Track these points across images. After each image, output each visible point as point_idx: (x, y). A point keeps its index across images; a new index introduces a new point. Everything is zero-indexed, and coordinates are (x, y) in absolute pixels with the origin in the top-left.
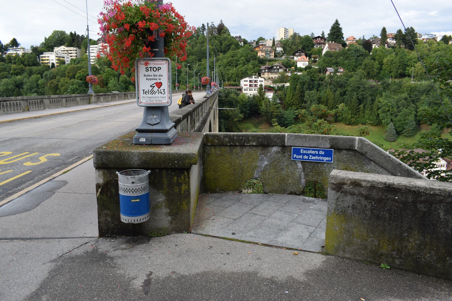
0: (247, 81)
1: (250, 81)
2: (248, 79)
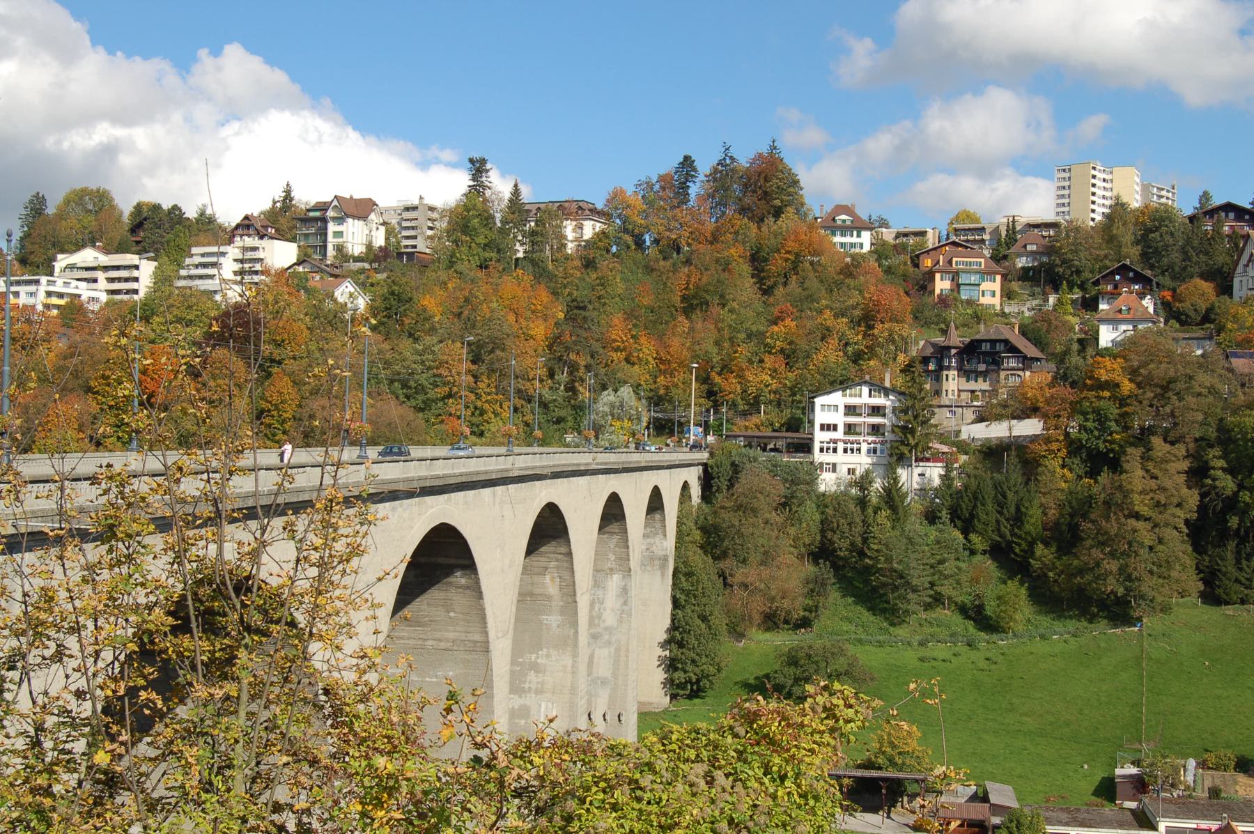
1: (851, 410)
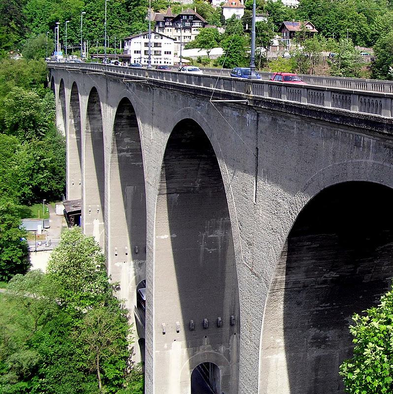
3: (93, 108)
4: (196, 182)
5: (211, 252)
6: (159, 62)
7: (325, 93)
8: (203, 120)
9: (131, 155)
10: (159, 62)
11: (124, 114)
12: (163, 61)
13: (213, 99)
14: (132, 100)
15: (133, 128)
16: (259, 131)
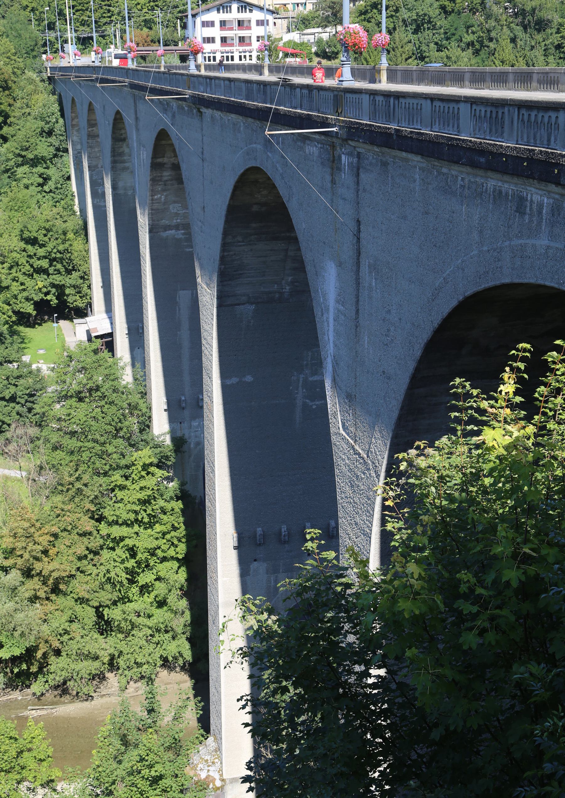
0: (212, 24)
2: (215, 16)
3: (121, 150)
4: (284, 282)
5: (314, 407)
6: (248, 58)
7: (462, 106)
8: (277, 169)
9: (183, 234)
10: (248, 58)
11: (165, 160)
12: (236, 56)
13: (269, 130)
14: (173, 131)
15: (404, 154)
16: (361, 188)
